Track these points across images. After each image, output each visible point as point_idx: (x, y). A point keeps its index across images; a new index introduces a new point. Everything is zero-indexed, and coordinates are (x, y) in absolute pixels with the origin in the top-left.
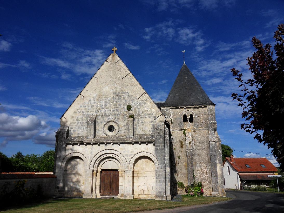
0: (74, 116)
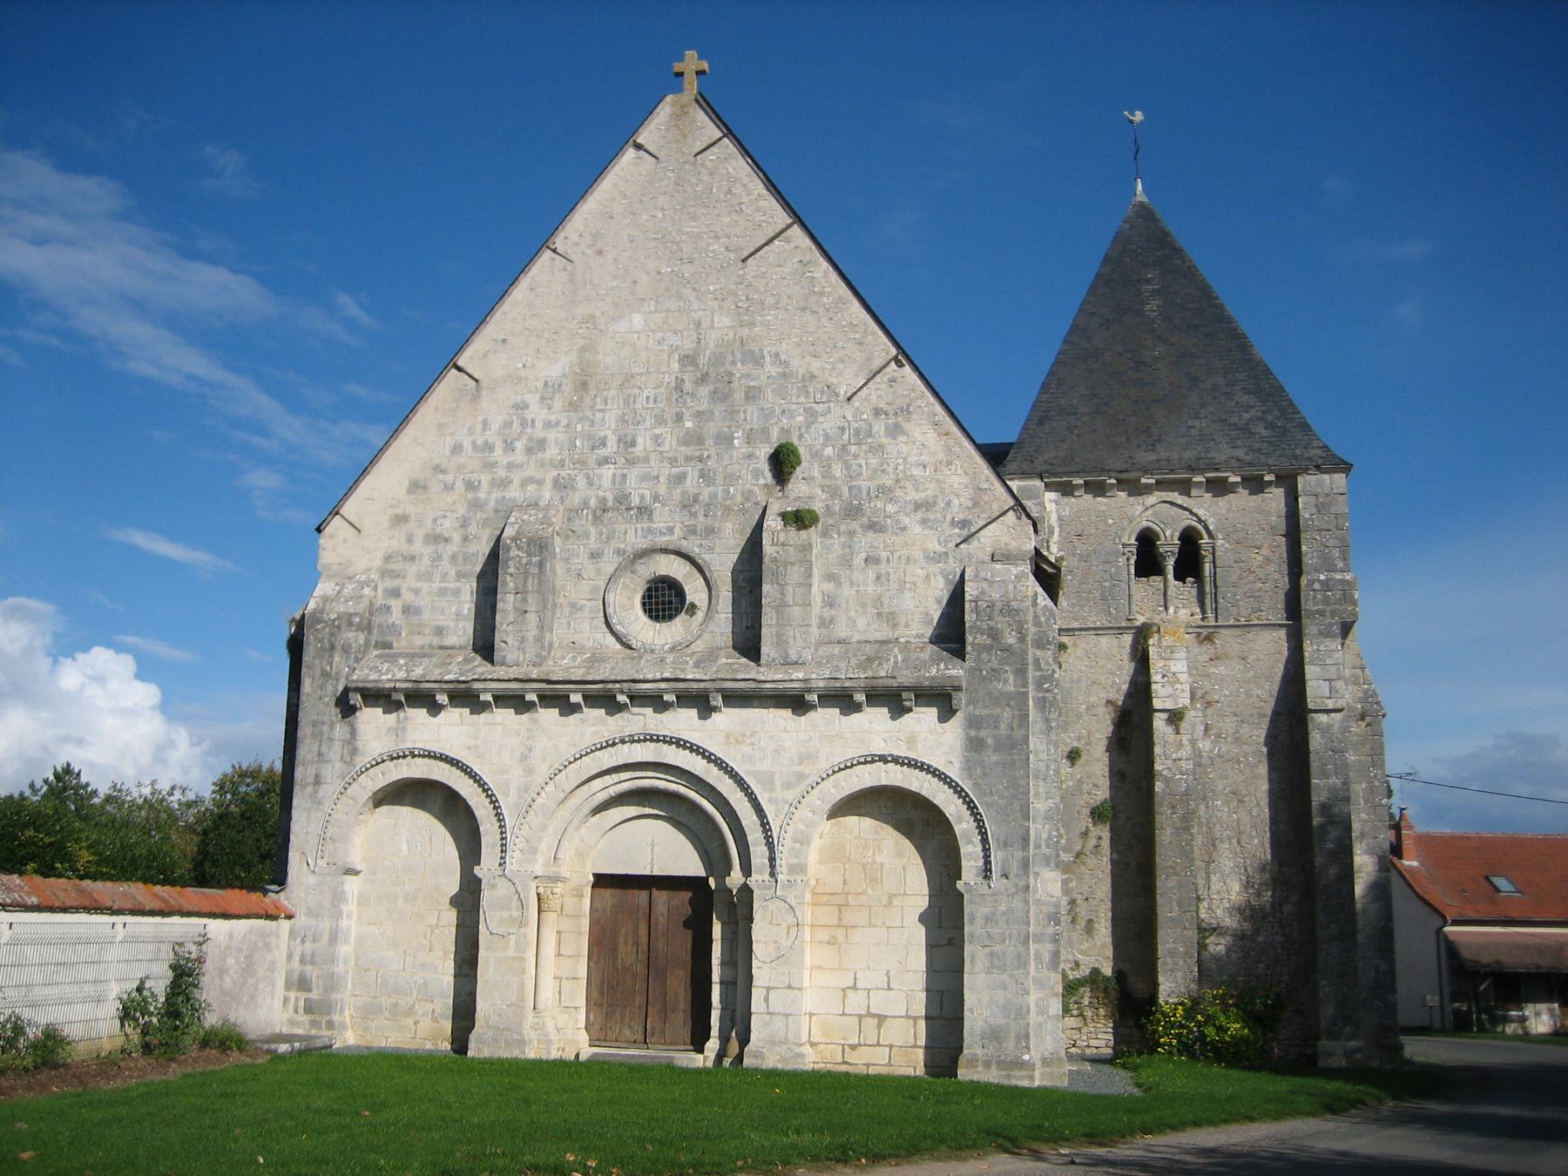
0: (410, 509)
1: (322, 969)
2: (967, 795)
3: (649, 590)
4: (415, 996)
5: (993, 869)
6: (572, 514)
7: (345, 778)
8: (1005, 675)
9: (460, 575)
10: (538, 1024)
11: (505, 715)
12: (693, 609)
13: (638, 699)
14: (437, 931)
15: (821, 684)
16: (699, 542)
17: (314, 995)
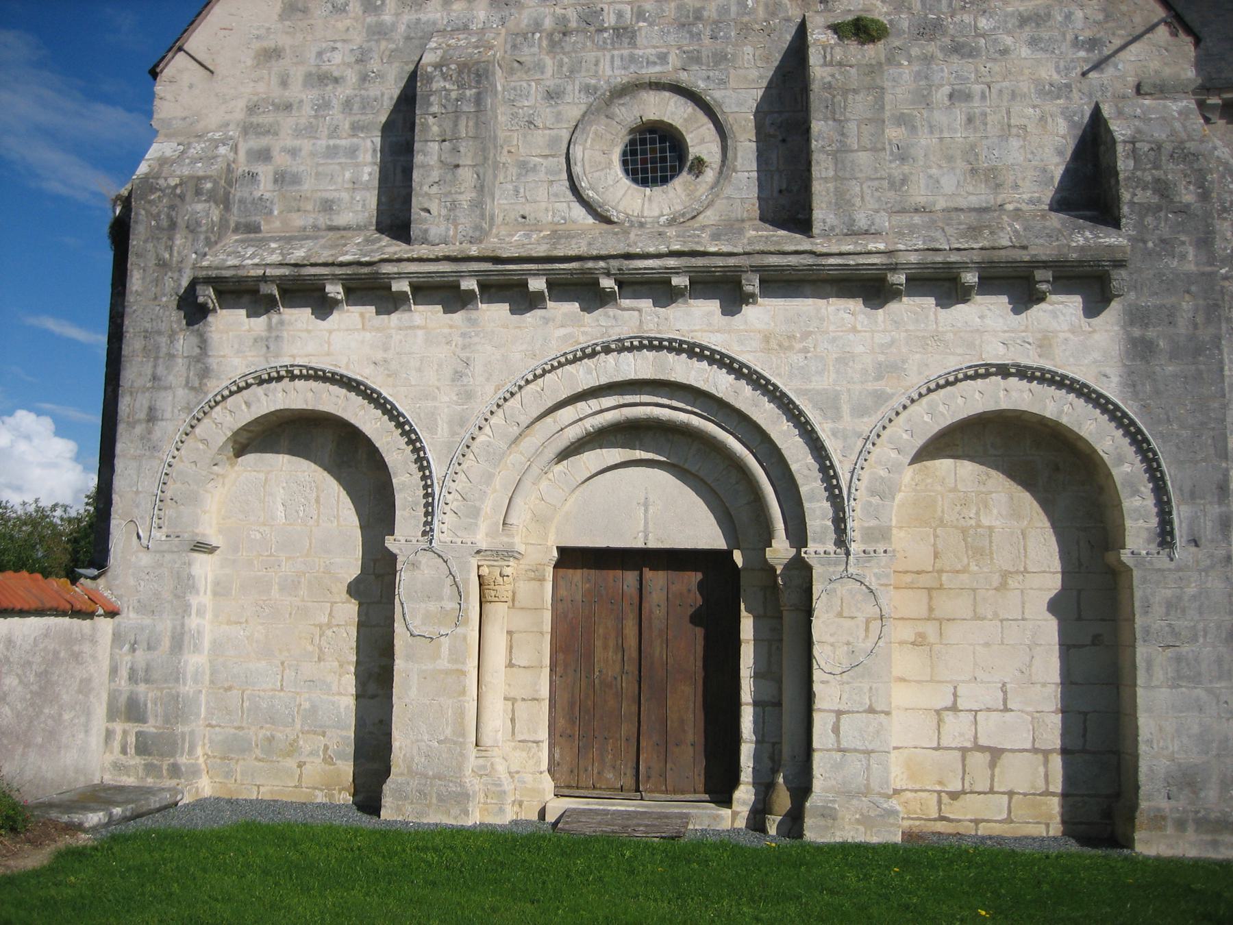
0: (284, 41)
1: (161, 690)
2: (1132, 423)
3: (632, 143)
4: (298, 726)
5: (1177, 532)
6: (520, 38)
7: (191, 410)
8: (1182, 249)
9: (356, 128)
10: (484, 767)
11: (427, 316)
12: (699, 166)
13: (634, 285)
14: (329, 633)
15: (913, 258)
16: (704, 74)
17: (150, 728)
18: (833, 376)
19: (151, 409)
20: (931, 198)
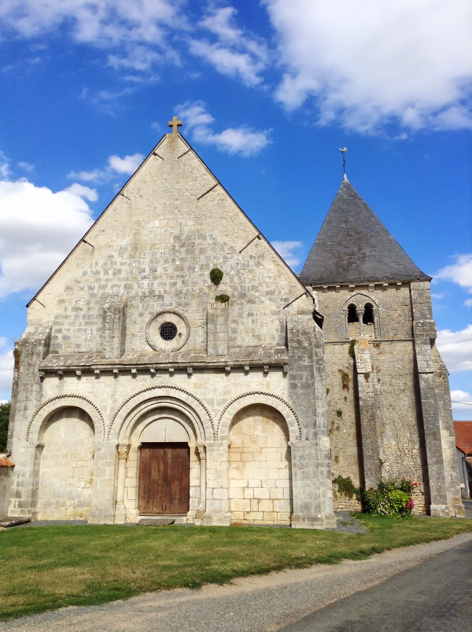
0: (65, 297)
14: (76, 469)
15: (232, 363)
17: (22, 499)
18: (212, 395)
19: (25, 407)
20: (242, 343)
